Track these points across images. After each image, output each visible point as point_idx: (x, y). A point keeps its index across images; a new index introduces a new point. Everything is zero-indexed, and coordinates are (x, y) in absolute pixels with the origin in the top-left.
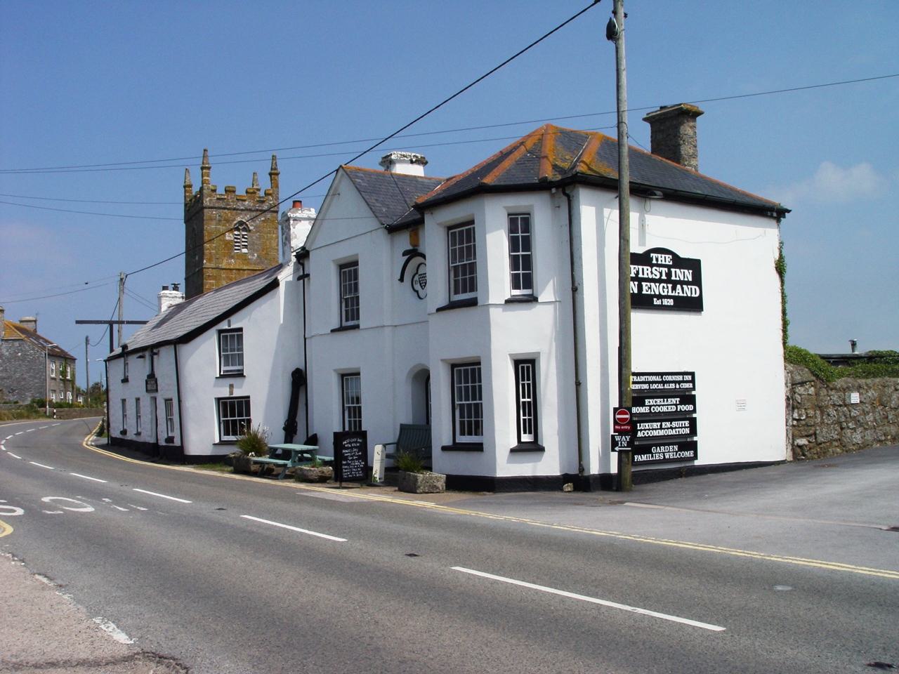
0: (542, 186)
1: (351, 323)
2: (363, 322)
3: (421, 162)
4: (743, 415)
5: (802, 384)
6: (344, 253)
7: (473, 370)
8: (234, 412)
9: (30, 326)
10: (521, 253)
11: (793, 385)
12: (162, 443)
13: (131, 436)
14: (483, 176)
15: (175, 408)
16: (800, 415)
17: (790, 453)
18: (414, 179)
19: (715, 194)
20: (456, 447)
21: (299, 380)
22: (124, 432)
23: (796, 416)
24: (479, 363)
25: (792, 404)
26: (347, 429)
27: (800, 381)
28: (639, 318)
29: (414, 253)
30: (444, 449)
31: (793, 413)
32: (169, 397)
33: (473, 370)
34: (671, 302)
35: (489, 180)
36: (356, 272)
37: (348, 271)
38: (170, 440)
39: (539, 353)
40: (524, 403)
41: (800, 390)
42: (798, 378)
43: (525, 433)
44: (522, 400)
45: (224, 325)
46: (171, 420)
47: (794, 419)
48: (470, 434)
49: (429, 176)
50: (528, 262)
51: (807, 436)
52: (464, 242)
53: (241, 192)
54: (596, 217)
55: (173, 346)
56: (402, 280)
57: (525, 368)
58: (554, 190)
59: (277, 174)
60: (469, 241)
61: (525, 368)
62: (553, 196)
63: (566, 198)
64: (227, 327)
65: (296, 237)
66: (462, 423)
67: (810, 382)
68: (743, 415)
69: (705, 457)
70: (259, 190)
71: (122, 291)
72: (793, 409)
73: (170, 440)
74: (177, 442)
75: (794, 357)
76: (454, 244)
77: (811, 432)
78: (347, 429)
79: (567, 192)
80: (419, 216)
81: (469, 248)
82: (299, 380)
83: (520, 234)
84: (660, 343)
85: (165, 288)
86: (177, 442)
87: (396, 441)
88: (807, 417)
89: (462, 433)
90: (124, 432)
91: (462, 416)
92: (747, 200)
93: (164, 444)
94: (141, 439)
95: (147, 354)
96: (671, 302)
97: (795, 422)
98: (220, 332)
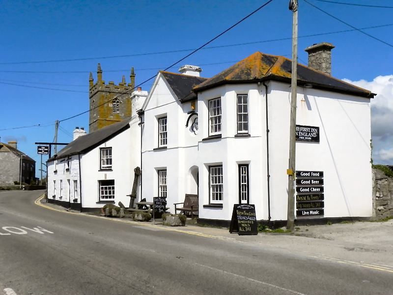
0: (255, 81)
1: (163, 146)
2: (168, 146)
3: (199, 70)
4: (349, 191)
5: (381, 179)
6: (160, 112)
7: (219, 169)
8: (107, 185)
9: (13, 146)
10: (243, 113)
11: (377, 180)
12: (72, 202)
13: (57, 198)
14: (225, 77)
15: (78, 184)
16: (380, 195)
17: (375, 214)
18: (195, 78)
19: (351, 89)
20: (210, 206)
21: (138, 173)
22: (54, 197)
23: (378, 195)
24: (222, 166)
25: (376, 189)
26: (160, 196)
27: (380, 178)
28: (298, 145)
29: (193, 113)
30: (205, 206)
31: (376, 193)
32: (76, 179)
33: (219, 169)
34: (310, 138)
35: (228, 78)
36: (166, 121)
37: (162, 119)
38: (76, 200)
39: (250, 161)
40: (243, 185)
41: (379, 182)
42: (379, 177)
43: (243, 199)
44: (242, 183)
45: (103, 146)
46: (76, 191)
47: (377, 197)
48: (217, 199)
49: (202, 77)
50: (246, 117)
51: (384, 205)
52: (215, 105)
53: (117, 84)
54: (279, 97)
55: (78, 156)
56: (187, 125)
57: (243, 167)
58: (259, 83)
59: (134, 76)
60: (218, 105)
61: (243, 167)
62: (259, 86)
63: (265, 87)
64: (104, 147)
65: (138, 104)
66: (213, 194)
67: (385, 178)
68: (349, 191)
69: (327, 214)
70: (125, 84)
71: (57, 129)
72: (376, 191)
73: (76, 200)
74: (79, 202)
75: (374, 167)
76: (241, 120)
77: (385, 203)
78: (160, 196)
79: (266, 84)
80: (196, 95)
81: (241, 120)
82: (138, 173)
83: (243, 104)
84: (309, 158)
85: (77, 128)
86: (79, 202)
87: (183, 202)
88: (383, 196)
89: (214, 199)
90: (54, 197)
91: (213, 190)
92: (354, 90)
93: (73, 202)
94: (63, 200)
95: (66, 159)
96: (310, 138)
97: (377, 198)
98: (101, 149)
